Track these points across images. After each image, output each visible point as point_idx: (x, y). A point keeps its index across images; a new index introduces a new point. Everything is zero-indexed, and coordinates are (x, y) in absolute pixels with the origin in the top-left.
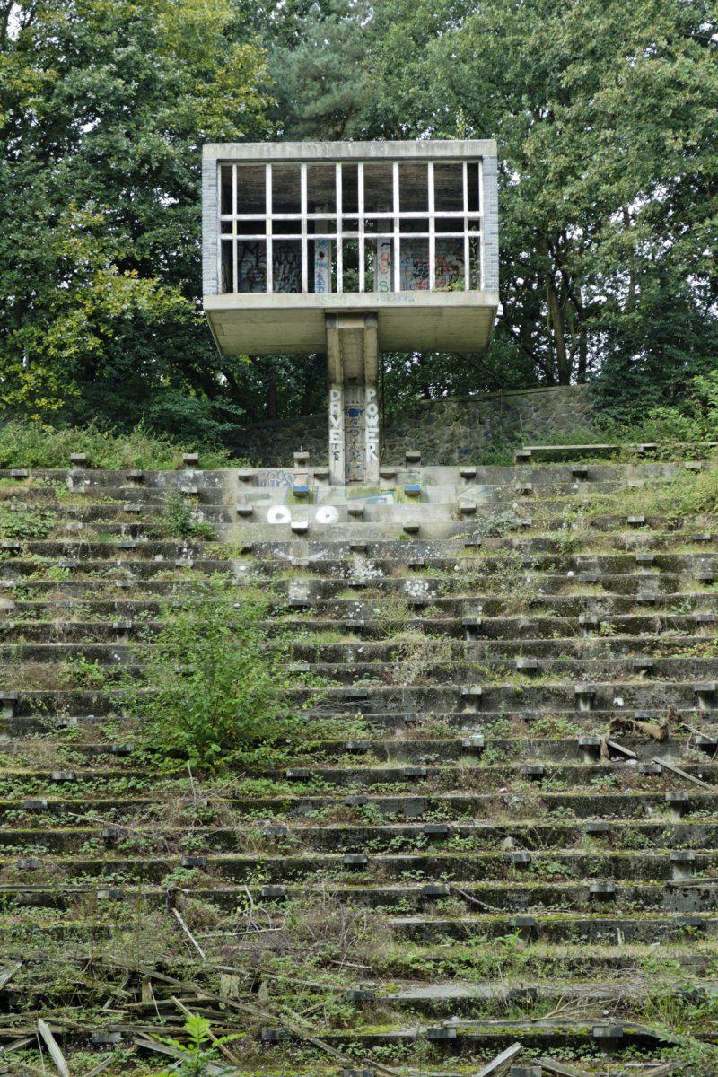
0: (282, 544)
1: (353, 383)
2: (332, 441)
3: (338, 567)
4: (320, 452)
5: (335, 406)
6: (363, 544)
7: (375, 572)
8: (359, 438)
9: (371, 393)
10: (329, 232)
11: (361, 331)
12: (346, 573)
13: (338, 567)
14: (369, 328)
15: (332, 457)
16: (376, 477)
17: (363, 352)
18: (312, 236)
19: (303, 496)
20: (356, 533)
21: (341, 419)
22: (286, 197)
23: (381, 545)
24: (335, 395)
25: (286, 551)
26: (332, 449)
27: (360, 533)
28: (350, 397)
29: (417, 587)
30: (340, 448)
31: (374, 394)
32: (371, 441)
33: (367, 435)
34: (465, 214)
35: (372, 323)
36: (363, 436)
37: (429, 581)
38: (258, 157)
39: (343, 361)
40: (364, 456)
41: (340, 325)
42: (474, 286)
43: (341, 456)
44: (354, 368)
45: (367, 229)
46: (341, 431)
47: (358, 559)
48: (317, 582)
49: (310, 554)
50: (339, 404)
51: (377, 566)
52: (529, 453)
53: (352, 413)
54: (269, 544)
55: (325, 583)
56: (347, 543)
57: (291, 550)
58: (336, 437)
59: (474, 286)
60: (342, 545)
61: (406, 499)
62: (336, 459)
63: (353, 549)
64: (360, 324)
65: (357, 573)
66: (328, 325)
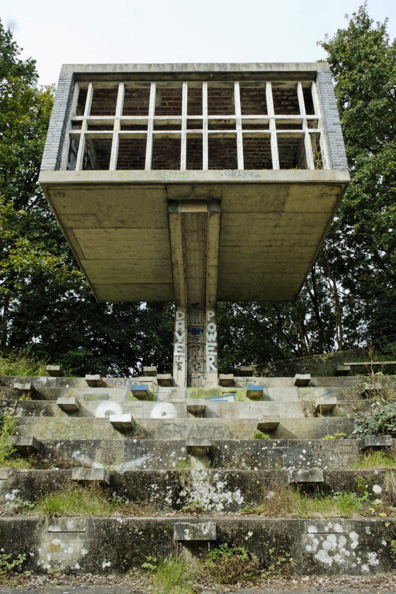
0: (87, 443)
1: (195, 308)
2: (175, 354)
3: (163, 485)
4: (166, 366)
5: (180, 325)
6: (206, 443)
7: (228, 495)
8: (200, 352)
9: (210, 314)
10: (176, 114)
11: (205, 216)
12: (176, 496)
13: (163, 485)
14: (213, 213)
15: (175, 368)
16: (215, 385)
17: (205, 257)
18: (152, 110)
19: (143, 396)
20: (196, 432)
21: (184, 335)
22: (133, 103)
23: (232, 445)
24: (180, 315)
25: (92, 456)
26: (176, 360)
27: (200, 430)
28: (193, 319)
29: (331, 542)
30: (183, 360)
31: (213, 314)
32: (211, 355)
33: (207, 348)
34: (184, 133)
35: (215, 208)
36: (204, 349)
37: (359, 527)
38: (111, 71)
39: (188, 289)
40: (205, 367)
41: (182, 210)
42: (319, 165)
43: (184, 366)
44: (197, 296)
45: (210, 127)
46: (184, 345)
47: (198, 467)
48: (107, 525)
49: (127, 460)
50: (183, 322)
51: (232, 484)
52: (349, 368)
53: (195, 332)
54: (67, 443)
55: (125, 528)
56: (182, 443)
57: (98, 453)
58: (179, 353)
59: (319, 165)
60: (176, 446)
61: (248, 400)
62: (179, 369)
63: (191, 450)
64: (203, 209)
65: (196, 496)
66: (171, 210)
